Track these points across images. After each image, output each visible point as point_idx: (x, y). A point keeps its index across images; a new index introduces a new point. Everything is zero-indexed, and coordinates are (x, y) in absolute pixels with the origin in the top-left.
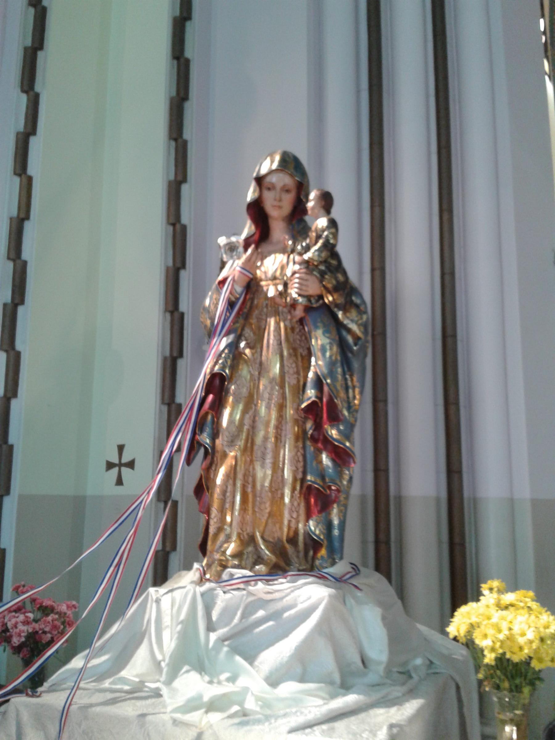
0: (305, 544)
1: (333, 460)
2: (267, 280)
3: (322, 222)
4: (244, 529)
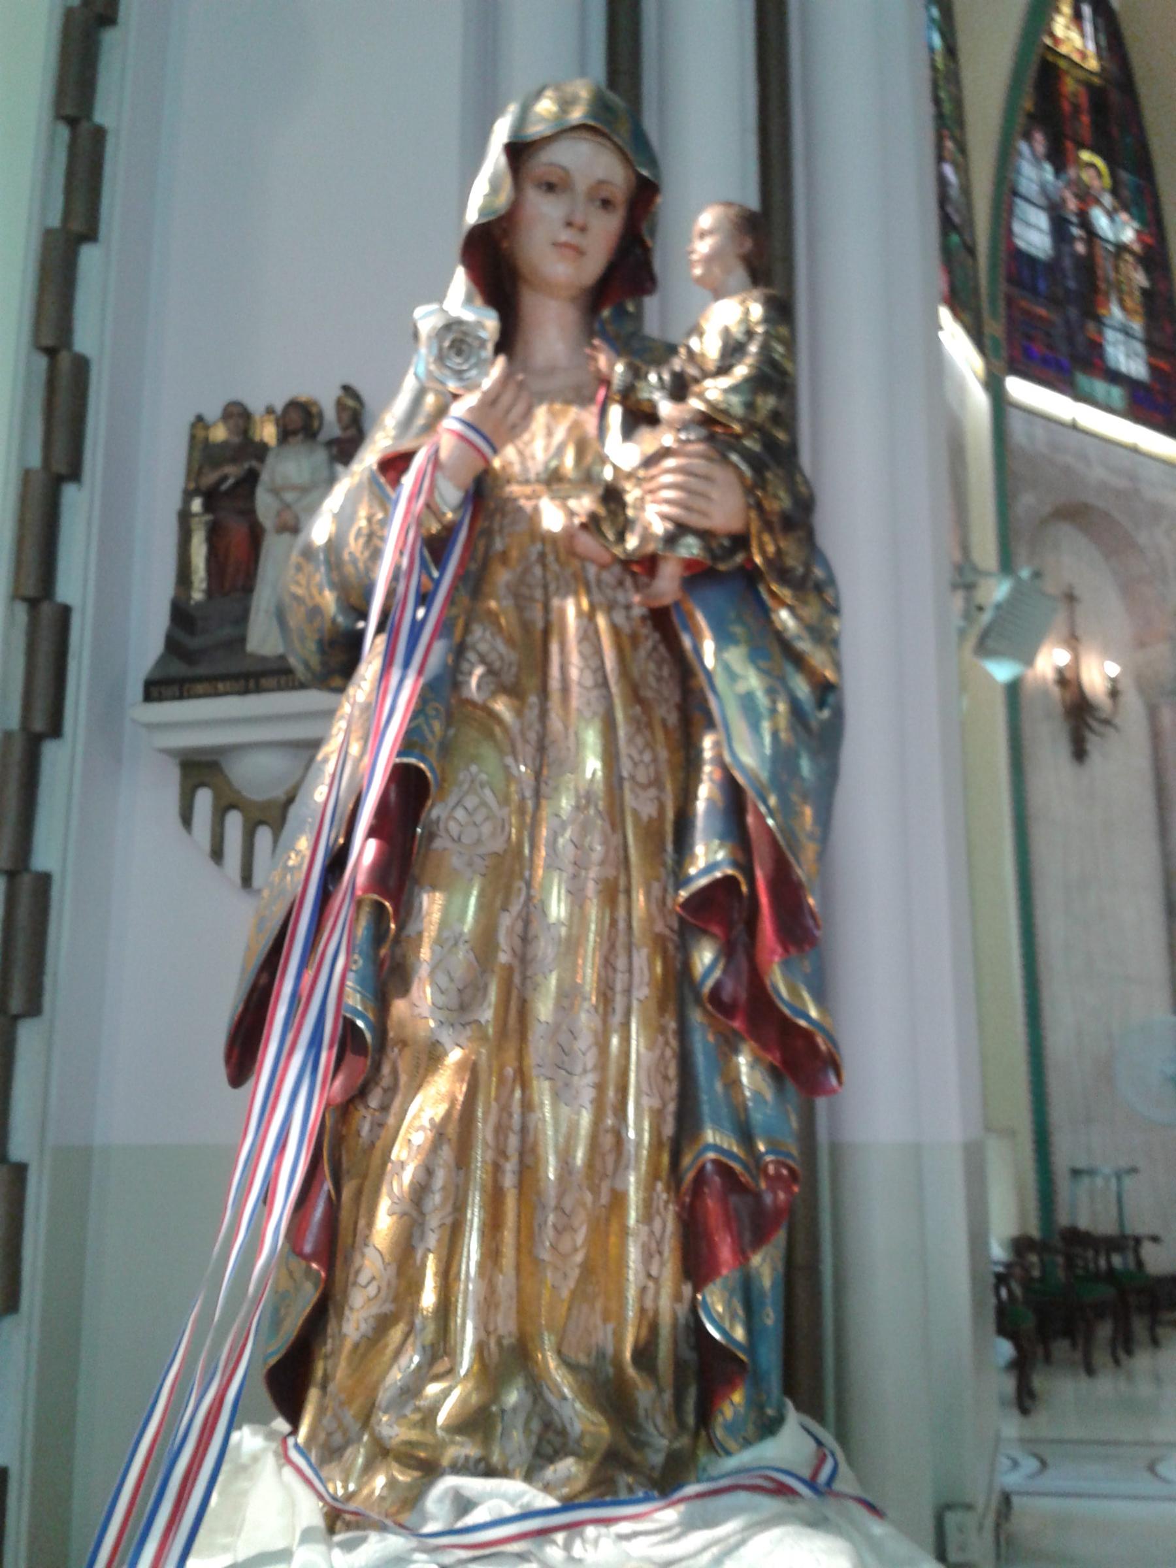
0: (679, 1365)
1: (776, 1075)
2: (527, 482)
3: (731, 314)
4: (491, 1328)
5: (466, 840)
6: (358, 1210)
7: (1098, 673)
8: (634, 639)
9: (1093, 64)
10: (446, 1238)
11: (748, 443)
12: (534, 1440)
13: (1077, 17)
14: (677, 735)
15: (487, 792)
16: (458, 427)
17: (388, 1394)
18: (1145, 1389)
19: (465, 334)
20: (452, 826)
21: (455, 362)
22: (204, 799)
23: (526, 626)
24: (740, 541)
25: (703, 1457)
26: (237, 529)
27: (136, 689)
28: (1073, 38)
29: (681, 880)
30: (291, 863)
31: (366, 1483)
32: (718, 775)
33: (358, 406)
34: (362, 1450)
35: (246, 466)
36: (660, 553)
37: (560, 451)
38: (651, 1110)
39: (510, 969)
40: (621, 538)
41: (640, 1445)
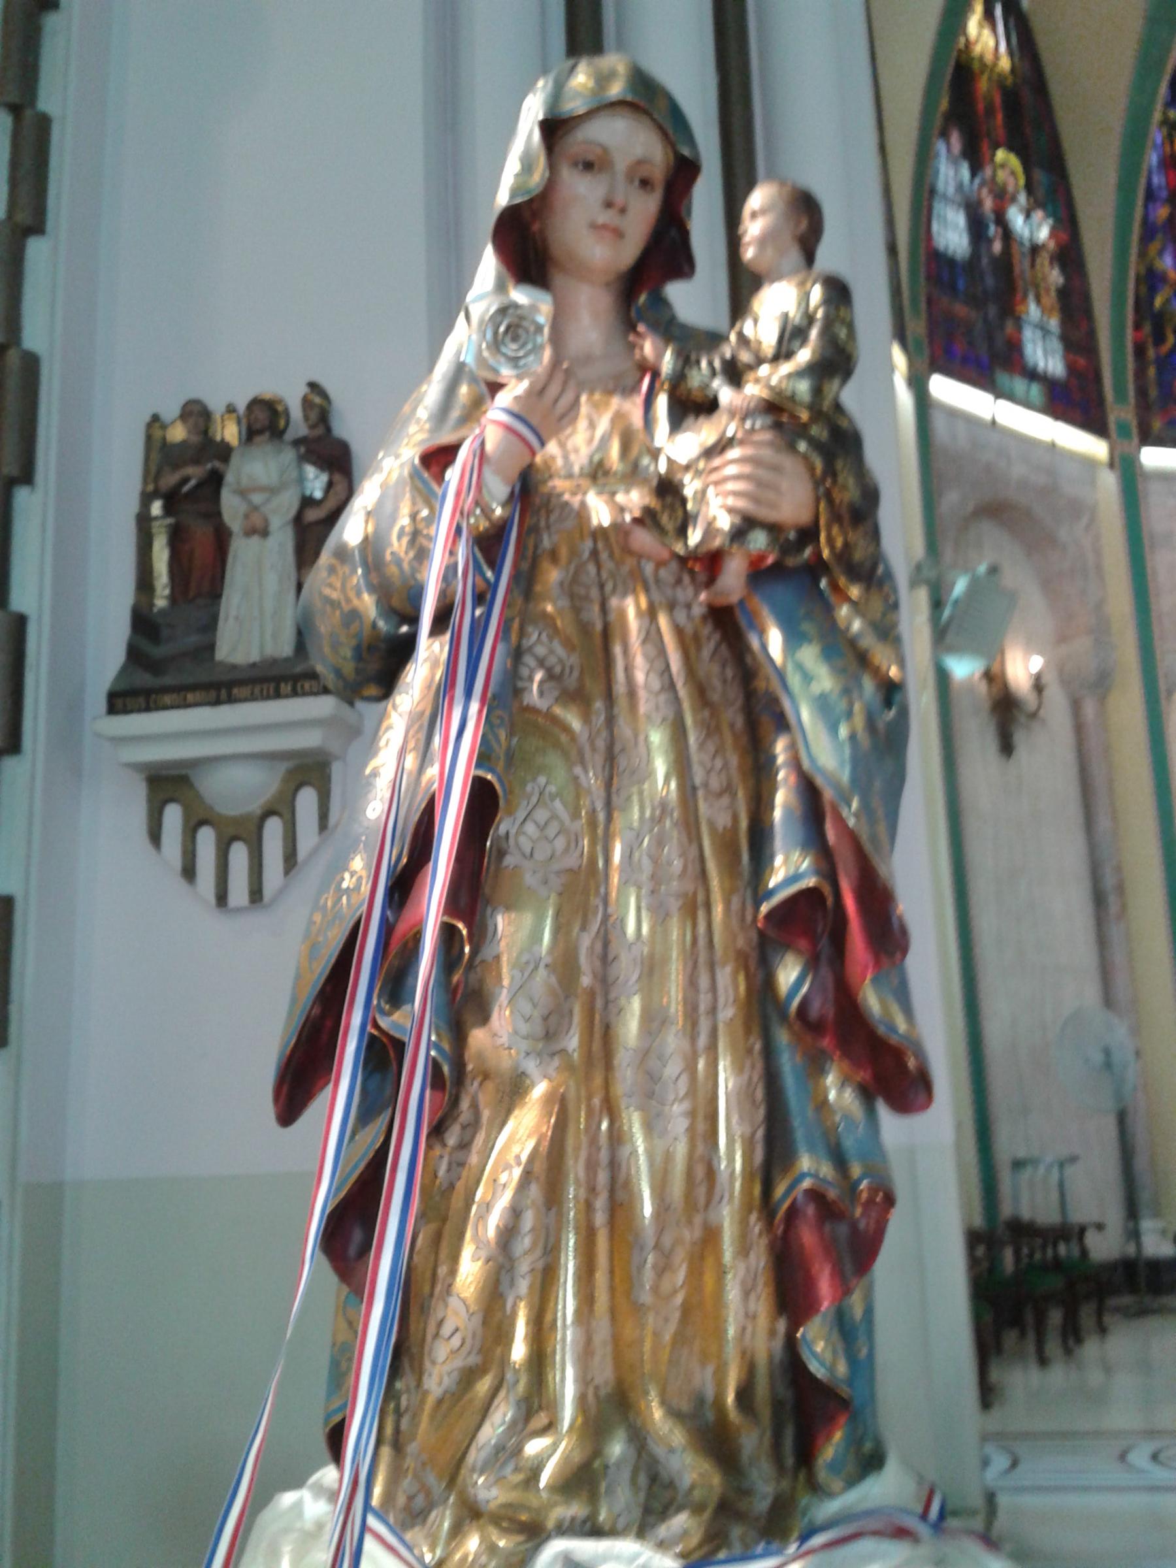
0: (777, 1405)
5: (540, 856)
6: (437, 1254)
7: (1022, 667)
8: (696, 637)
9: (1005, 64)
10: (539, 1281)
11: (815, 430)
12: (642, 1496)
13: (989, 15)
14: (744, 740)
15: (558, 804)
16: (505, 418)
17: (483, 1455)
18: (1095, 1377)
19: (521, 318)
20: (522, 840)
21: (511, 348)
22: (173, 816)
23: (584, 629)
24: (808, 534)
25: (804, 1500)
26: (201, 532)
27: (97, 699)
28: (985, 38)
29: (759, 892)
30: (345, 885)
31: (457, 1548)
32: (793, 779)
33: (325, 404)
34: (448, 1513)
35: (209, 466)
36: (726, 548)
37: (605, 441)
38: (742, 1136)
39: (591, 993)
40: (682, 532)
41: (746, 1493)
